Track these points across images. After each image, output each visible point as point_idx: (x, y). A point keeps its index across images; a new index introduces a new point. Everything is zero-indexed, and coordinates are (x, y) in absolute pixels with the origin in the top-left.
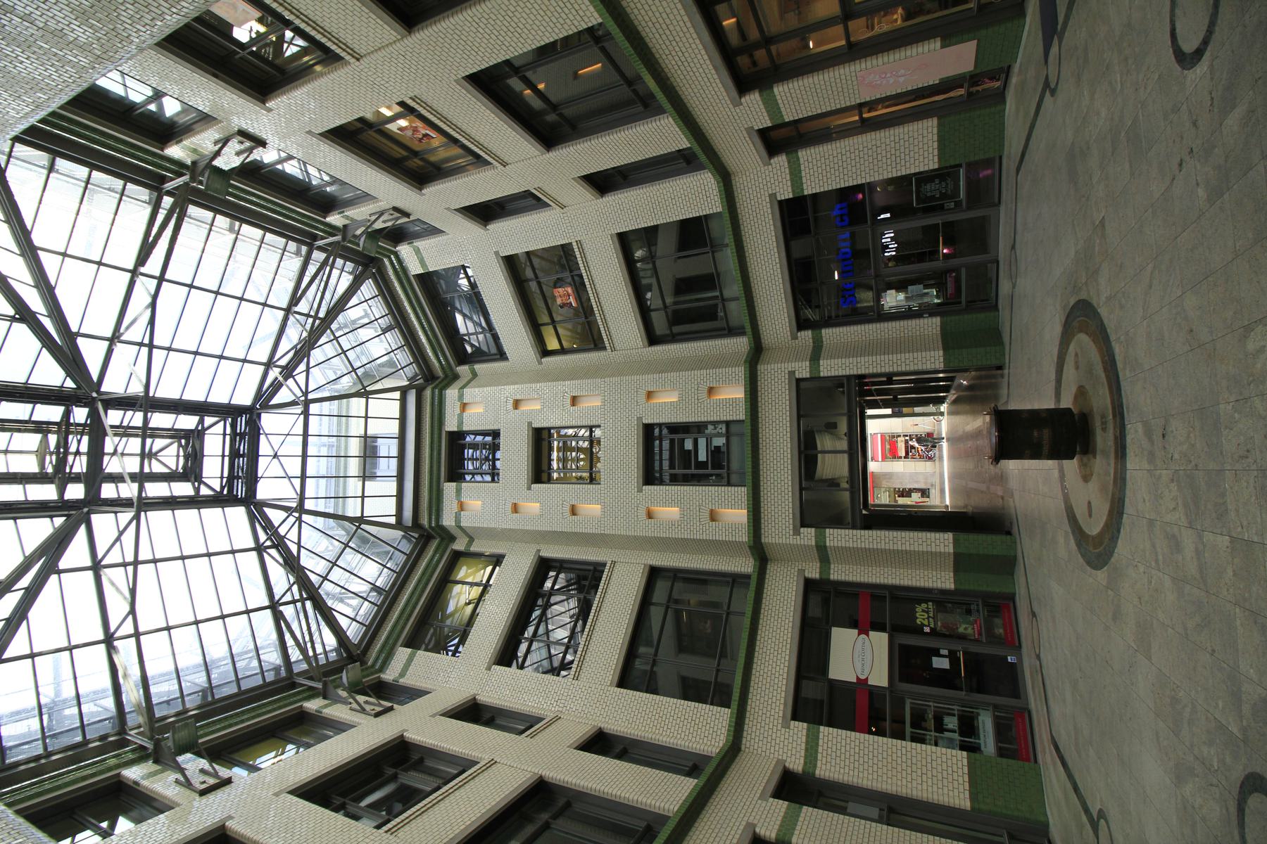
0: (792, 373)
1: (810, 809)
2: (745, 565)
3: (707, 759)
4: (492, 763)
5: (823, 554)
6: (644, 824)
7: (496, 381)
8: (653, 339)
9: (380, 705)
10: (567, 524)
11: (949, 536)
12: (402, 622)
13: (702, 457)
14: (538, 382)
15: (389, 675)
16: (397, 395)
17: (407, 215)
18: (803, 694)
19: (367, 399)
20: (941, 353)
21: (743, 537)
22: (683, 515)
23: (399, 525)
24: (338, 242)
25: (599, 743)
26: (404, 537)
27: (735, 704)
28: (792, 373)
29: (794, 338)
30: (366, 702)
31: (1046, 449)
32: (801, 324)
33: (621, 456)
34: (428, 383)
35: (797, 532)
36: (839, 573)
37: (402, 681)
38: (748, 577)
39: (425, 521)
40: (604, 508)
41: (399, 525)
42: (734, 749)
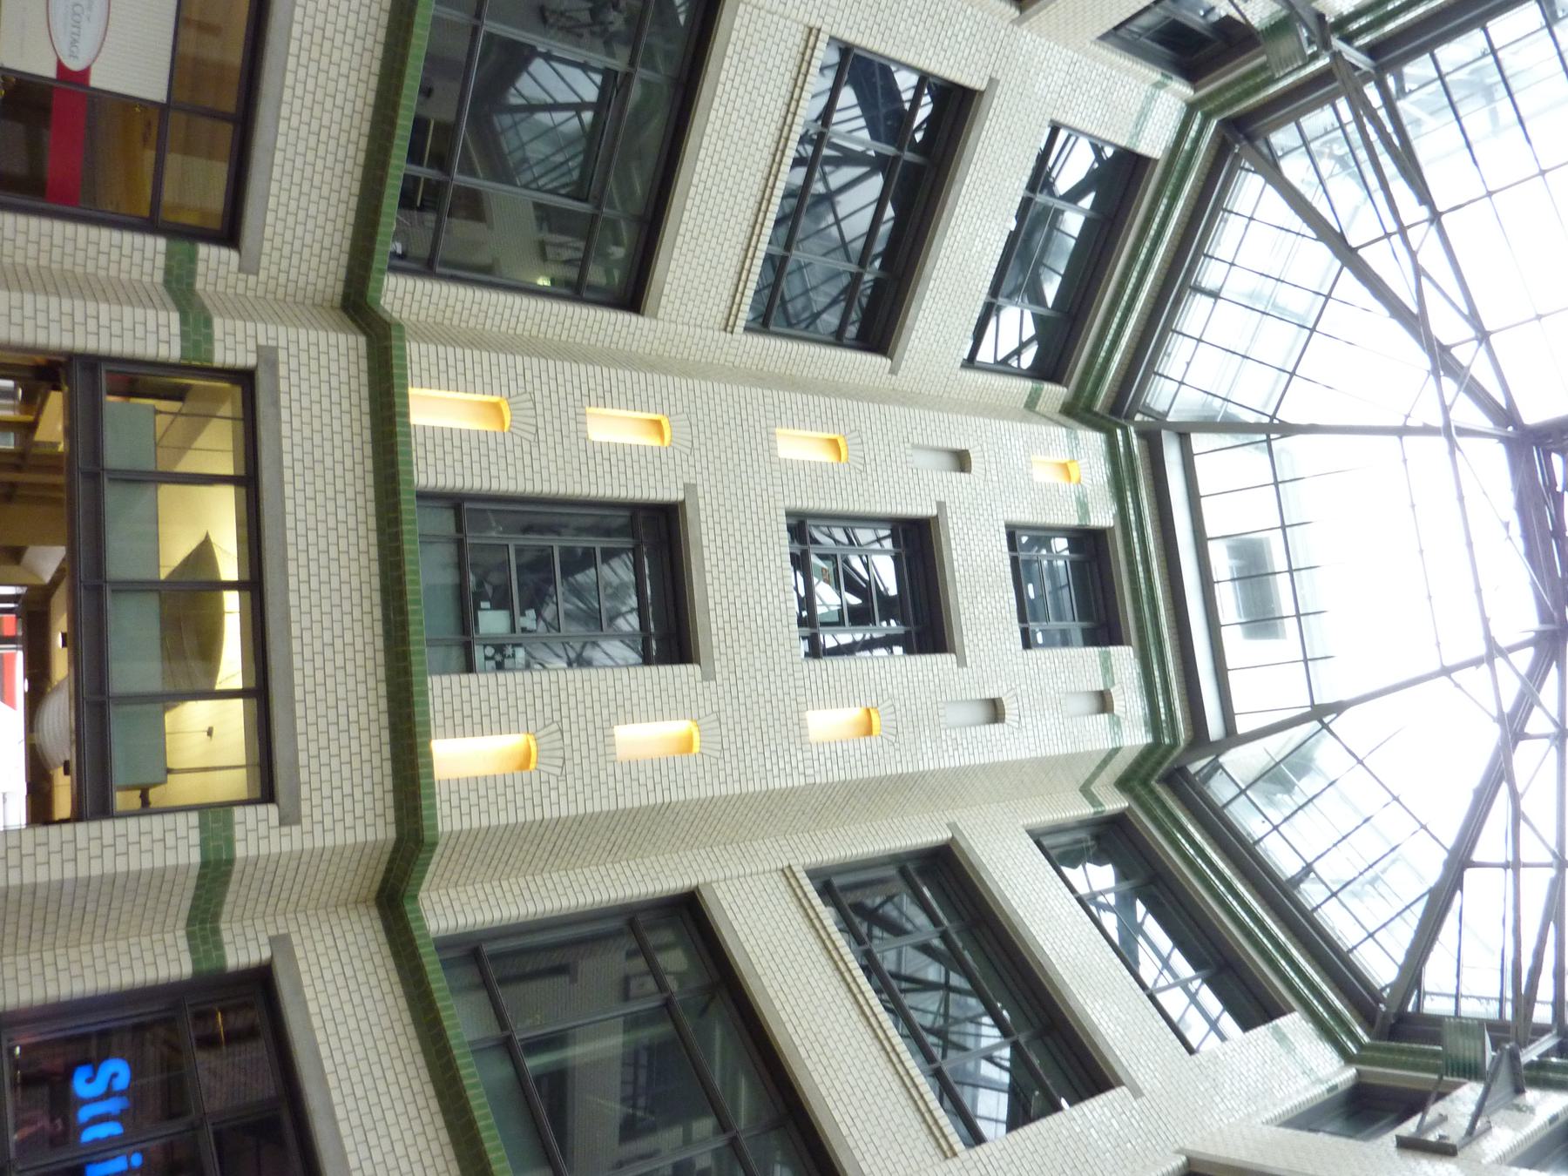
0: (289, 818)
2: (400, 295)
7: (1047, 768)
16: (1243, 726)
17: (1405, 1144)
18: (219, 172)
19: (1313, 705)
21: (416, 354)
22: (580, 420)
24: (1525, 1043)
26: (1166, 414)
28: (289, 818)
29: (280, 942)
32: (260, 985)
33: (744, 580)
34: (1173, 768)
35: (268, 355)
36: (146, 253)
38: (393, 269)
40: (771, 450)
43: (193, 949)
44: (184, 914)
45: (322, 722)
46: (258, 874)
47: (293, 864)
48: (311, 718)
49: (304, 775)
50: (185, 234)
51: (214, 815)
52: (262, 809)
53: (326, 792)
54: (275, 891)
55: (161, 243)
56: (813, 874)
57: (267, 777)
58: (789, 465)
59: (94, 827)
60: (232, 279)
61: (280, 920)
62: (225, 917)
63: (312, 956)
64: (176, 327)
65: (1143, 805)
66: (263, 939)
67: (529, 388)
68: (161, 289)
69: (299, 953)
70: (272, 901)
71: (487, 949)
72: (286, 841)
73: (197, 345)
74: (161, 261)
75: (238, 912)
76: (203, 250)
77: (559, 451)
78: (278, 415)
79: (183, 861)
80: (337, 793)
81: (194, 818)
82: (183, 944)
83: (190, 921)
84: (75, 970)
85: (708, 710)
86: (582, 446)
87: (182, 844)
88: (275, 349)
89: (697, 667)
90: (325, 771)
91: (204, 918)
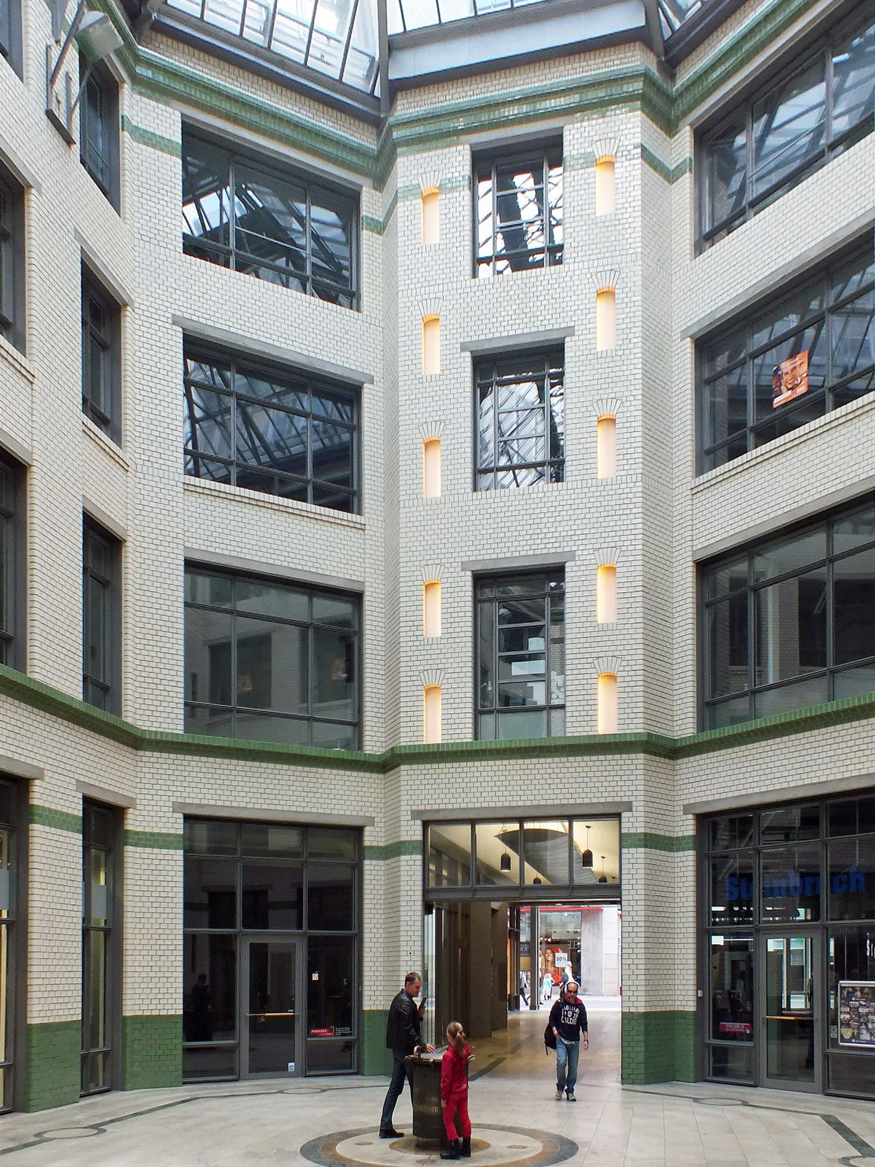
1: (80, 843)
2: (374, 744)
3: (116, 708)
4: (29, 378)
5: (393, 851)
6: (10, 633)
8: (706, 567)
9: (70, 111)
10: (409, 436)
11: (73, 1011)
12: (226, 106)
13: (518, 669)
14: (645, 338)
15: (133, 105)
20: (642, 1010)
21: (406, 740)
22: (432, 642)
23: (392, 46)
25: (102, 545)
27: (188, 739)
28: (629, 806)
29: (687, 809)
30: (68, 79)
31: (421, 1108)
33: (519, 524)
35: (415, 815)
36: (373, 870)
37: (125, 137)
38: (360, 747)
39: (406, 107)
41: (392, 46)
42: (135, 741)
43: (684, 850)
44: (667, 853)
45: (586, 790)
46: (653, 821)
47: (650, 804)
48: (584, 795)
49: (610, 800)
50: (360, 852)
51: (624, 841)
52: (623, 820)
53: (618, 789)
54: (662, 812)
55: (367, 862)
56: (700, 471)
57: (611, 814)
58: (445, 488)
59: (624, 892)
60: (378, 829)
61: (677, 808)
62: (672, 835)
63: (695, 795)
64: (408, 857)
65: (685, 114)
66: (684, 817)
67: (417, 673)
68: (387, 862)
69: (692, 801)
70: (667, 813)
71: (708, 698)
72: (639, 809)
73: (414, 848)
74: (374, 862)
75: (670, 829)
76: (367, 843)
77: (449, 655)
78: (443, 810)
79: (642, 856)
80: (620, 783)
81: (624, 850)
82: (681, 854)
83: (671, 850)
84: (684, 899)
85: (592, 557)
86: (445, 641)
87: (636, 856)
88: (412, 811)
89: (567, 564)
90: (609, 789)
91: (668, 844)
